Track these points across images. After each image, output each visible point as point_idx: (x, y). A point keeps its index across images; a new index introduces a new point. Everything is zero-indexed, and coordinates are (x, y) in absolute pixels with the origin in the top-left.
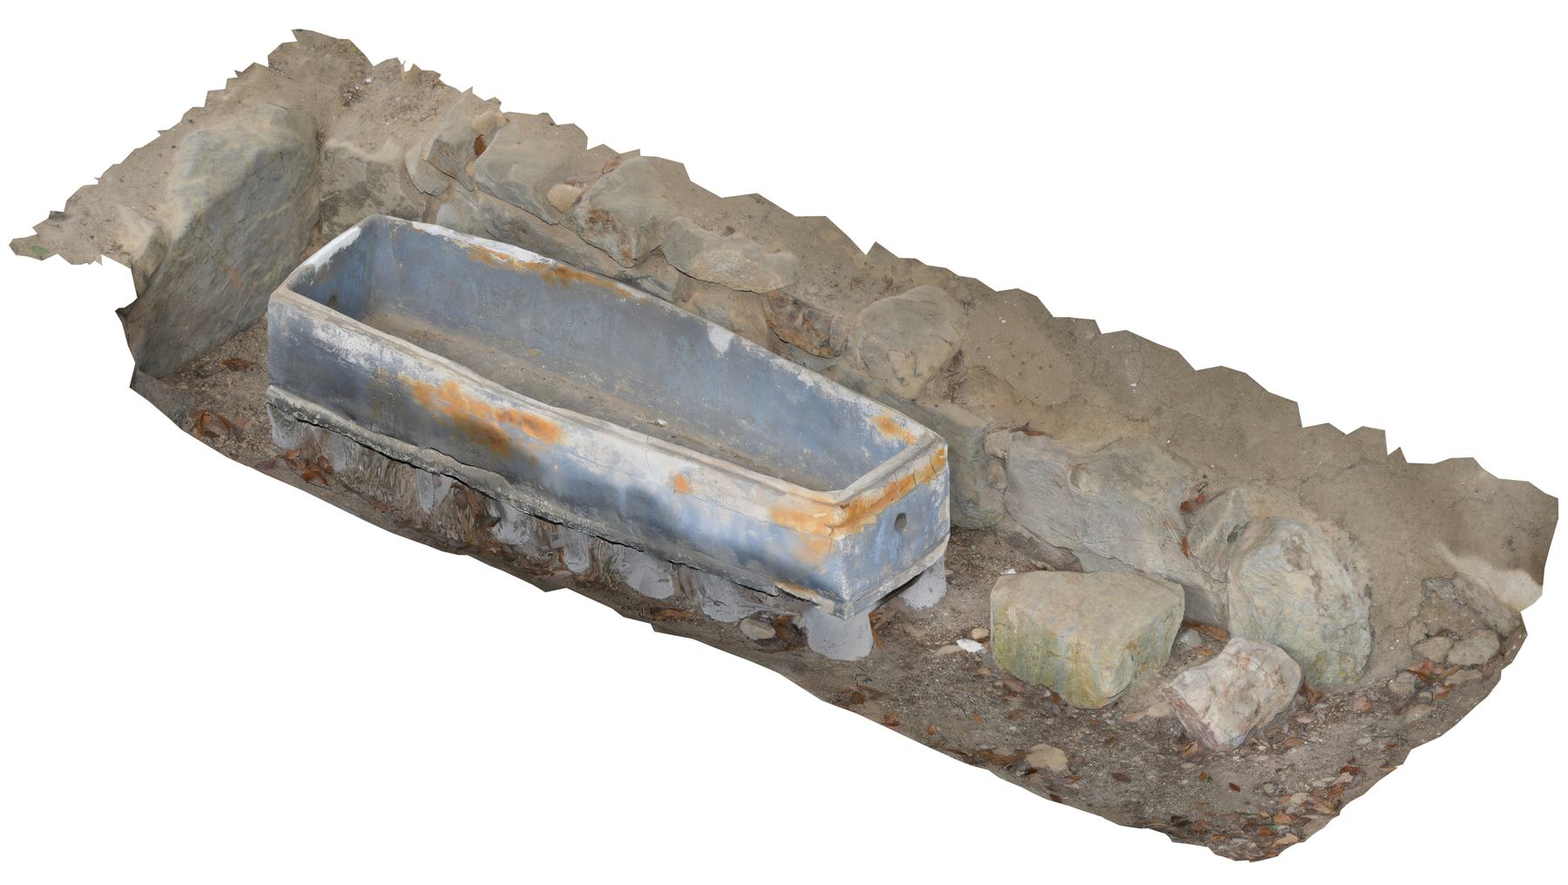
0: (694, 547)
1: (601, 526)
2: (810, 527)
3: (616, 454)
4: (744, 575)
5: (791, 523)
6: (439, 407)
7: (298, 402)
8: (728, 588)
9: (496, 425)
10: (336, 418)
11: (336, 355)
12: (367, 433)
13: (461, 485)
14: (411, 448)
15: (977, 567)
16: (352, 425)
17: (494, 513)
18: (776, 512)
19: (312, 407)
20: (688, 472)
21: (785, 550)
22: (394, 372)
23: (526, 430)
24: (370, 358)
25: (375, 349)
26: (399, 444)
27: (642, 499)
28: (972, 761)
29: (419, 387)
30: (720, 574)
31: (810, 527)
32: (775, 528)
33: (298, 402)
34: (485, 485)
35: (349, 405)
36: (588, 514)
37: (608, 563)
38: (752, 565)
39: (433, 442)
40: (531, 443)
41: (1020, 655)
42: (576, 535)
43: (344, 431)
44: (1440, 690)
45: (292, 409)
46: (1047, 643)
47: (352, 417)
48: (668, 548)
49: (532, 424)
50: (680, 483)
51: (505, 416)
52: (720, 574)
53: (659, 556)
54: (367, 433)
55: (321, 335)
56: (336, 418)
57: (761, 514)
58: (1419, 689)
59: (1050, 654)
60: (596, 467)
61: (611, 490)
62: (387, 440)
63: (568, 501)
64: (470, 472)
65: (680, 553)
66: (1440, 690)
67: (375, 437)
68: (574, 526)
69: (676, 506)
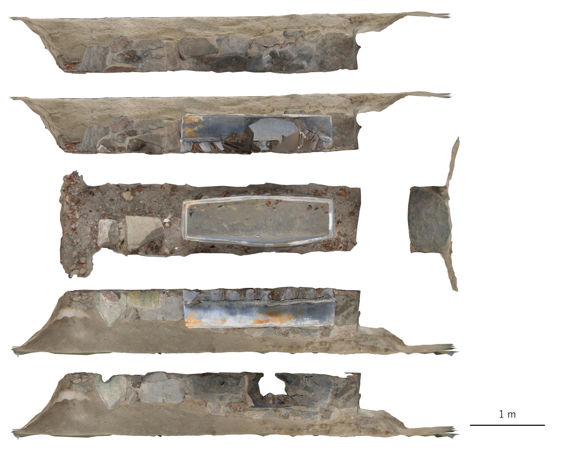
0: (221, 306)
1: (244, 303)
2: (192, 321)
3: (239, 322)
4: (209, 303)
5: (197, 320)
6: (285, 316)
7: (324, 301)
8: (212, 298)
9: (270, 318)
10: (313, 302)
11: (313, 318)
12: (305, 301)
13: (279, 300)
14: (293, 303)
15: (183, 245)
16: (309, 301)
17: (270, 296)
18: (201, 322)
19: (320, 301)
20: (222, 324)
21: (200, 313)
22: (297, 320)
23: (262, 320)
24: (303, 321)
25: (302, 323)
26: (296, 302)
27: (233, 314)
28: (153, 290)
29: (290, 319)
30: (215, 301)
31: (192, 321)
32: (201, 318)
33: (324, 301)
34: (272, 302)
35: (309, 307)
36: (246, 305)
37: (241, 295)
38: (207, 306)
39: (287, 307)
40: (261, 317)
41: (151, 297)
42: (250, 299)
43: (311, 299)
44: (75, 262)
45: (325, 298)
46: (144, 303)
47: (309, 304)
48: (227, 303)
49: (261, 322)
50: (224, 321)
51: (267, 321)
52: (215, 301)
53: (229, 301)
54: (305, 301)
55: (317, 321)
56: (313, 302)
57: (204, 320)
58: (79, 260)
59: (143, 301)
60: (245, 317)
61: (241, 313)
62: (299, 302)
63: (251, 306)
64: (277, 303)
65: (225, 303)
66: (75, 262)
67: (303, 301)
68: (250, 301)
69: (225, 315)
